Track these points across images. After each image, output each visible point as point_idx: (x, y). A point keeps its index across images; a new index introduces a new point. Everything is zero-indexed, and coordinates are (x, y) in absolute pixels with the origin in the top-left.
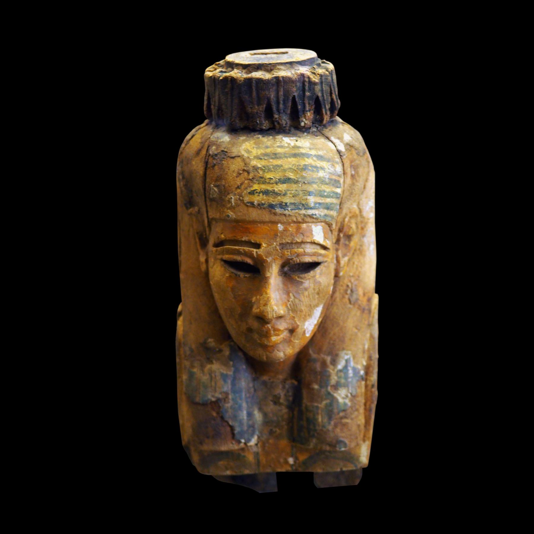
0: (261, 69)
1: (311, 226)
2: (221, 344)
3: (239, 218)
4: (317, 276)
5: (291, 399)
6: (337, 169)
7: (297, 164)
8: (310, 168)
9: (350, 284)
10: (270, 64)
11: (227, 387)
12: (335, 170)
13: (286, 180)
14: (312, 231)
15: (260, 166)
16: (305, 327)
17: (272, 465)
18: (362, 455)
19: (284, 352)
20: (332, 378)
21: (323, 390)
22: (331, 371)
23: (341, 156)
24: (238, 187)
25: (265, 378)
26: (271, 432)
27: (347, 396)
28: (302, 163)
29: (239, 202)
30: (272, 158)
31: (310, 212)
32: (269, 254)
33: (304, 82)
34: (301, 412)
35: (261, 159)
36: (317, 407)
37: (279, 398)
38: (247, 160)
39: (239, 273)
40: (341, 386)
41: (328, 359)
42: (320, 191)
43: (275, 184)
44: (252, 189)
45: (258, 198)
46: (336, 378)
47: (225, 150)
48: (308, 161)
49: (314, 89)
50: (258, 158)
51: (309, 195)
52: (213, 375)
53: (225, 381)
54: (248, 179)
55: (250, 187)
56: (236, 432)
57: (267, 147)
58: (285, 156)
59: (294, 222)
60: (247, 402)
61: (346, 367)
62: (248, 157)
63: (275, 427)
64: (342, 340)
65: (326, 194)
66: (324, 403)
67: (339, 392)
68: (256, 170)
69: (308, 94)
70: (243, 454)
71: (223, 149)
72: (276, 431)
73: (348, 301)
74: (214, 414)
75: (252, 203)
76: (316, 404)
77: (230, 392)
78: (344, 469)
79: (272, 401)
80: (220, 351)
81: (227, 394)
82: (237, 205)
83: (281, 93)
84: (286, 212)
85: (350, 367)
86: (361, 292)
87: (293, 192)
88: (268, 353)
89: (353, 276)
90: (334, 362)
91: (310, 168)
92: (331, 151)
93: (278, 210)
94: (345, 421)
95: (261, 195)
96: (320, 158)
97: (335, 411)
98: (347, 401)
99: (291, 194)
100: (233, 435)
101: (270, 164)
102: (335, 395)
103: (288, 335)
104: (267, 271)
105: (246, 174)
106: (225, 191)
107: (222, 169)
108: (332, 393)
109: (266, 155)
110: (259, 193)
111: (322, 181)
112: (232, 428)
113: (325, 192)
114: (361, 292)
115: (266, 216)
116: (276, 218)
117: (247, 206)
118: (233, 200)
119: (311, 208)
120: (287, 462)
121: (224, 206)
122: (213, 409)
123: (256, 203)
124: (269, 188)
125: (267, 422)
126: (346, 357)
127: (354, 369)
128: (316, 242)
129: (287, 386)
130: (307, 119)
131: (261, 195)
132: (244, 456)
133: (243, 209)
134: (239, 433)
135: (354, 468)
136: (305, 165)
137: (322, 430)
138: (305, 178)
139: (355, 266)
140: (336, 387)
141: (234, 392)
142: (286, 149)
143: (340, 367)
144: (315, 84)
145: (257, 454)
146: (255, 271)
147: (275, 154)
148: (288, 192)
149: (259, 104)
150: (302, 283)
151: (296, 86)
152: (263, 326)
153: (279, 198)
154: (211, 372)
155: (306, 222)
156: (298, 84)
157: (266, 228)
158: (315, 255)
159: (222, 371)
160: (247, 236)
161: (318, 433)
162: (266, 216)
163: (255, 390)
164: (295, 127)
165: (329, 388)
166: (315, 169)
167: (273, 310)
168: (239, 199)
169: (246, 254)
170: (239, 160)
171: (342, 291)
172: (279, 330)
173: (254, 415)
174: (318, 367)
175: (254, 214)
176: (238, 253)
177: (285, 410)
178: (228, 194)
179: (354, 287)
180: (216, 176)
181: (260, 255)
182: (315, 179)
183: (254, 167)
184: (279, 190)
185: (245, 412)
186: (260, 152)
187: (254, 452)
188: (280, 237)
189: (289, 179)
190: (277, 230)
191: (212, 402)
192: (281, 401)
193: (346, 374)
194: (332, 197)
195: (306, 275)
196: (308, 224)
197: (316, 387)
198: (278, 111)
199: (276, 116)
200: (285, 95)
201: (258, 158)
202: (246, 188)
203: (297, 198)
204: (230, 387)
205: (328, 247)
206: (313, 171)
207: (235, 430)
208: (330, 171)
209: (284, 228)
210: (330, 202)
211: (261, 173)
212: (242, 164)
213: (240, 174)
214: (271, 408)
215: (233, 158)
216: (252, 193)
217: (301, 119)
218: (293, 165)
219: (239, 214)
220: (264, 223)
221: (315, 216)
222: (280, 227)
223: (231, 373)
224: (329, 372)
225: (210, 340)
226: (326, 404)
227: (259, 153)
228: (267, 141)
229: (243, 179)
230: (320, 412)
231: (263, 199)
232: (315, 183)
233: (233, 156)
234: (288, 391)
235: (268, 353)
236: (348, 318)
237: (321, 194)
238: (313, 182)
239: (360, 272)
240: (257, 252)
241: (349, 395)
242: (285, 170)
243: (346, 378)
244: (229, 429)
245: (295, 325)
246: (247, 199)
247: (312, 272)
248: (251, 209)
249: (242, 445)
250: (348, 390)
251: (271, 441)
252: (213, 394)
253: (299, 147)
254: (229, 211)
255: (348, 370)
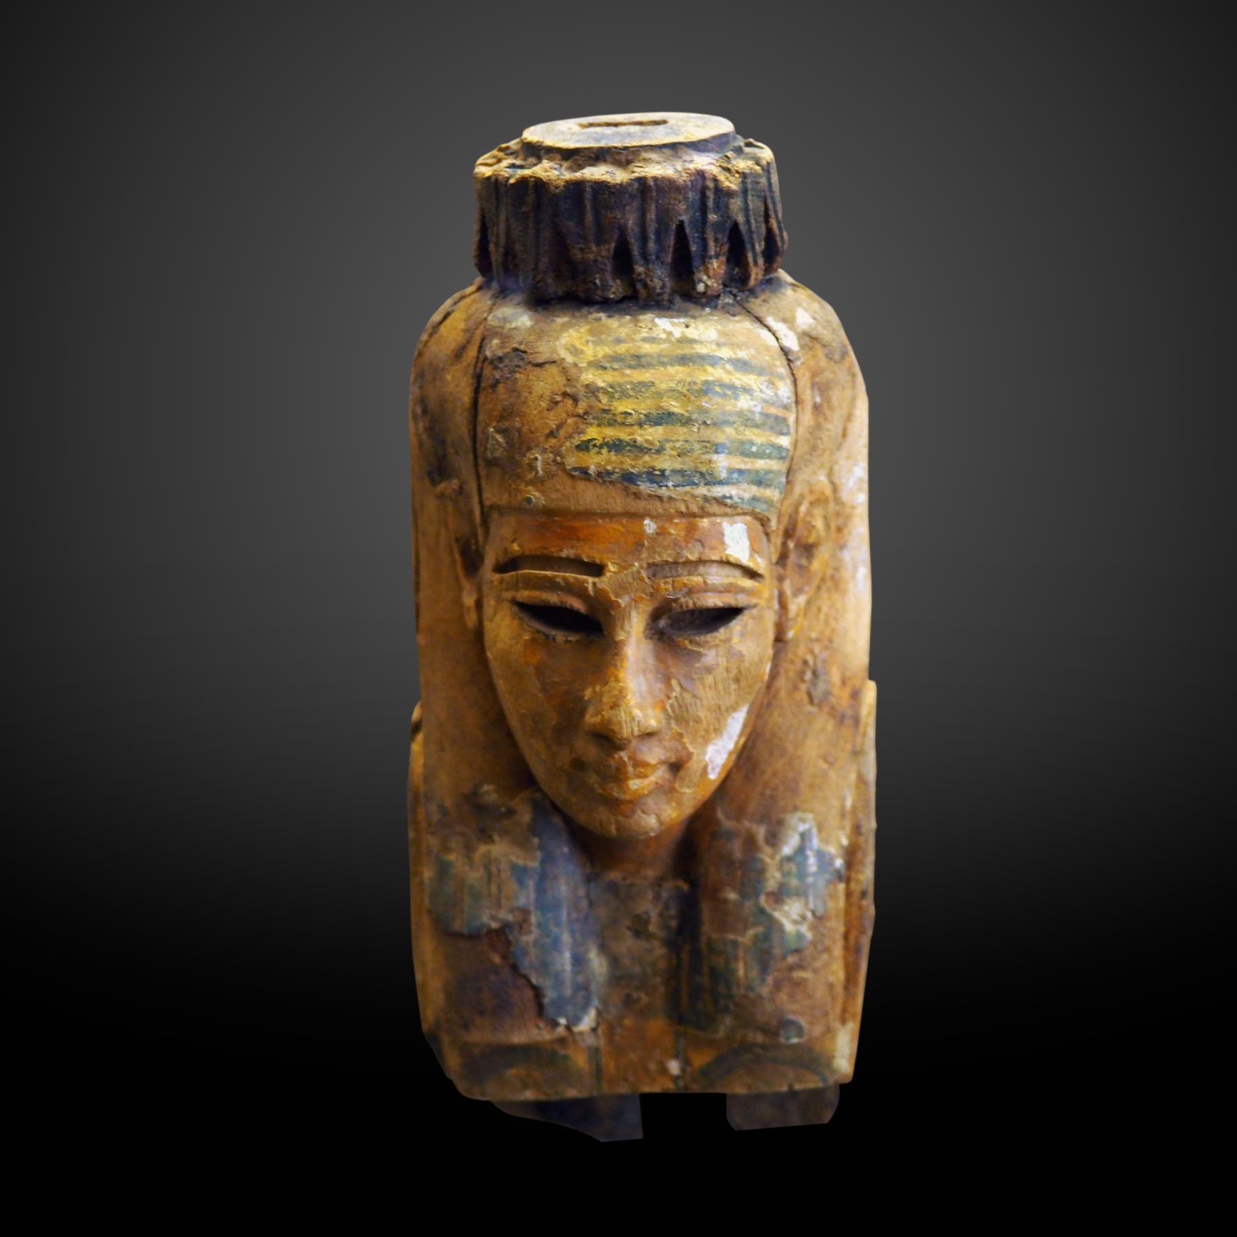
0: (605, 161)
1: (720, 524)
2: (512, 797)
3: (553, 506)
4: (735, 640)
5: (674, 923)
6: (780, 393)
7: (689, 380)
8: (718, 389)
9: (810, 658)
10: (626, 148)
11: (526, 897)
12: (776, 395)
13: (663, 418)
14: (723, 534)
15: (601, 384)
16: (707, 758)
17: (631, 1078)
18: (838, 1054)
19: (658, 816)
20: (768, 875)
21: (749, 904)
22: (767, 860)
23: (789, 361)
24: (552, 434)
25: (614, 875)
26: (628, 1002)
27: (804, 918)
28: (700, 377)
29: (554, 468)
30: (630, 367)
31: (718, 491)
32: (623, 588)
33: (704, 190)
34: (696, 955)
35: (605, 368)
36: (735, 944)
37: (646, 922)
38: (573, 371)
39: (553, 632)
40: (789, 895)
41: (761, 832)
42: (742, 443)
43: (636, 427)
44: (585, 438)
45: (597, 459)
46: (778, 875)
47: (522, 347)
48: (714, 373)
49: (727, 206)
50: (598, 365)
51: (717, 452)
52: (494, 869)
53: (521, 883)
54: (573, 416)
55: (579, 433)
56: (546, 1001)
57: (618, 341)
58: (661, 361)
59: (681, 514)
60: (572, 932)
61: (801, 850)
62: (575, 365)
63: (638, 989)
64: (793, 787)
65: (754, 449)
66: (751, 932)
67: (786, 908)
68: (593, 393)
69: (713, 217)
70: (562, 1052)
71: (516, 345)
72: (639, 999)
73: (806, 698)
74: (497, 959)
75: (584, 471)
76: (731, 937)
77: (532, 909)
78: (797, 1087)
79: (629, 928)
80: (511, 813)
81: (525, 912)
82: (550, 476)
83: (652, 216)
84: (663, 492)
85: (811, 849)
86: (836, 677)
87: (678, 445)
88: (621, 818)
89: (817, 640)
90: (774, 839)
91: (718, 389)
92: (768, 349)
93: (645, 487)
94: (798, 974)
95: (604, 451)
96: (742, 365)
97: (777, 951)
98: (804, 929)
99: (673, 448)
100: (540, 1007)
101: (626, 379)
102: (777, 914)
103: (668, 776)
104: (618, 629)
105: (569, 402)
106: (522, 443)
107: (513, 390)
108: (769, 910)
109: (616, 358)
110: (601, 447)
111: (747, 420)
112: (538, 992)
113: (752, 444)
114: (836, 677)
115: (617, 501)
116: (640, 505)
117: (573, 477)
118: (539, 464)
119: (721, 483)
120: (664, 1071)
121: (519, 477)
122: (494, 948)
123: (592, 470)
124: (624, 435)
125: (618, 978)
126: (802, 827)
127: (820, 855)
128: (732, 560)
129: (665, 895)
130: (711, 276)
131: (604, 451)
132: (566, 1057)
133: (562, 485)
134: (555, 1003)
135: (821, 1085)
136: (706, 382)
137: (746, 996)
138: (706, 411)
139: (822, 616)
140: (779, 896)
141: (542, 907)
142: (663, 346)
143: (787, 850)
144: (730, 194)
145: (594, 1052)
146: (592, 627)
147: (638, 357)
148: (668, 446)
149: (600, 241)
150: (699, 655)
151: (686, 199)
152: (610, 755)
153: (647, 458)
154: (488, 863)
155: (709, 515)
156: (691, 195)
157: (615, 527)
158: (729, 591)
159: (514, 859)
160: (572, 547)
161: (736, 1004)
162: (617, 501)
163: (591, 904)
164: (684, 295)
165: (762, 899)
166: (729, 393)
167: (633, 719)
168: (554, 461)
169: (570, 589)
170: (553, 370)
171: (792, 674)
172: (646, 765)
173: (589, 960)
174: (737, 849)
175: (588, 496)
176: (552, 585)
177: (660, 951)
178: (529, 449)
179: (819, 664)
180: (499, 407)
181: (602, 590)
182: (730, 414)
183: (587, 386)
184: (647, 441)
185: (567, 955)
186: (602, 351)
187: (589, 1048)
188: (648, 549)
189: (670, 414)
190: (643, 533)
191: (491, 932)
192: (652, 928)
193: (802, 866)
194: (769, 457)
195: (709, 637)
196: (713, 519)
197: (732, 896)
198: (645, 256)
199: (640, 269)
200: (659, 221)
201: (598, 365)
202: (570, 437)
203: (688, 459)
204: (532, 896)
205: (761, 571)
206: (724, 396)
207: (544, 996)
208: (764, 396)
209: (659, 528)
210: (765, 467)
211: (604, 400)
212: (561, 380)
213: (556, 403)
214: (627, 944)
215: (540, 365)
216: (584, 447)
217: (697, 276)
218: (679, 382)
219: (554, 496)
220: (610, 515)
221: (729, 501)
222: (650, 526)
223: (534, 864)
224: (762, 861)
225: (486, 788)
226: (756, 936)
227: (600, 355)
228: (619, 326)
229: (564, 415)
230: (741, 953)
231: (609, 462)
232: (730, 424)
233: (540, 360)
234: (667, 907)
235: (621, 818)
236: (806, 736)
237: (743, 450)
238: (726, 422)
239: (833, 631)
240: (594, 584)
241: (809, 915)
242: (659, 395)
243: (802, 875)
244: (529, 994)
245: (684, 754)
246: (571, 461)
247: (722, 630)
248: (581, 485)
249: (561, 1031)
250: (807, 904)
251: (628, 1022)
252: (494, 912)
253: (692, 341)
254: (530, 488)
255: (806, 858)
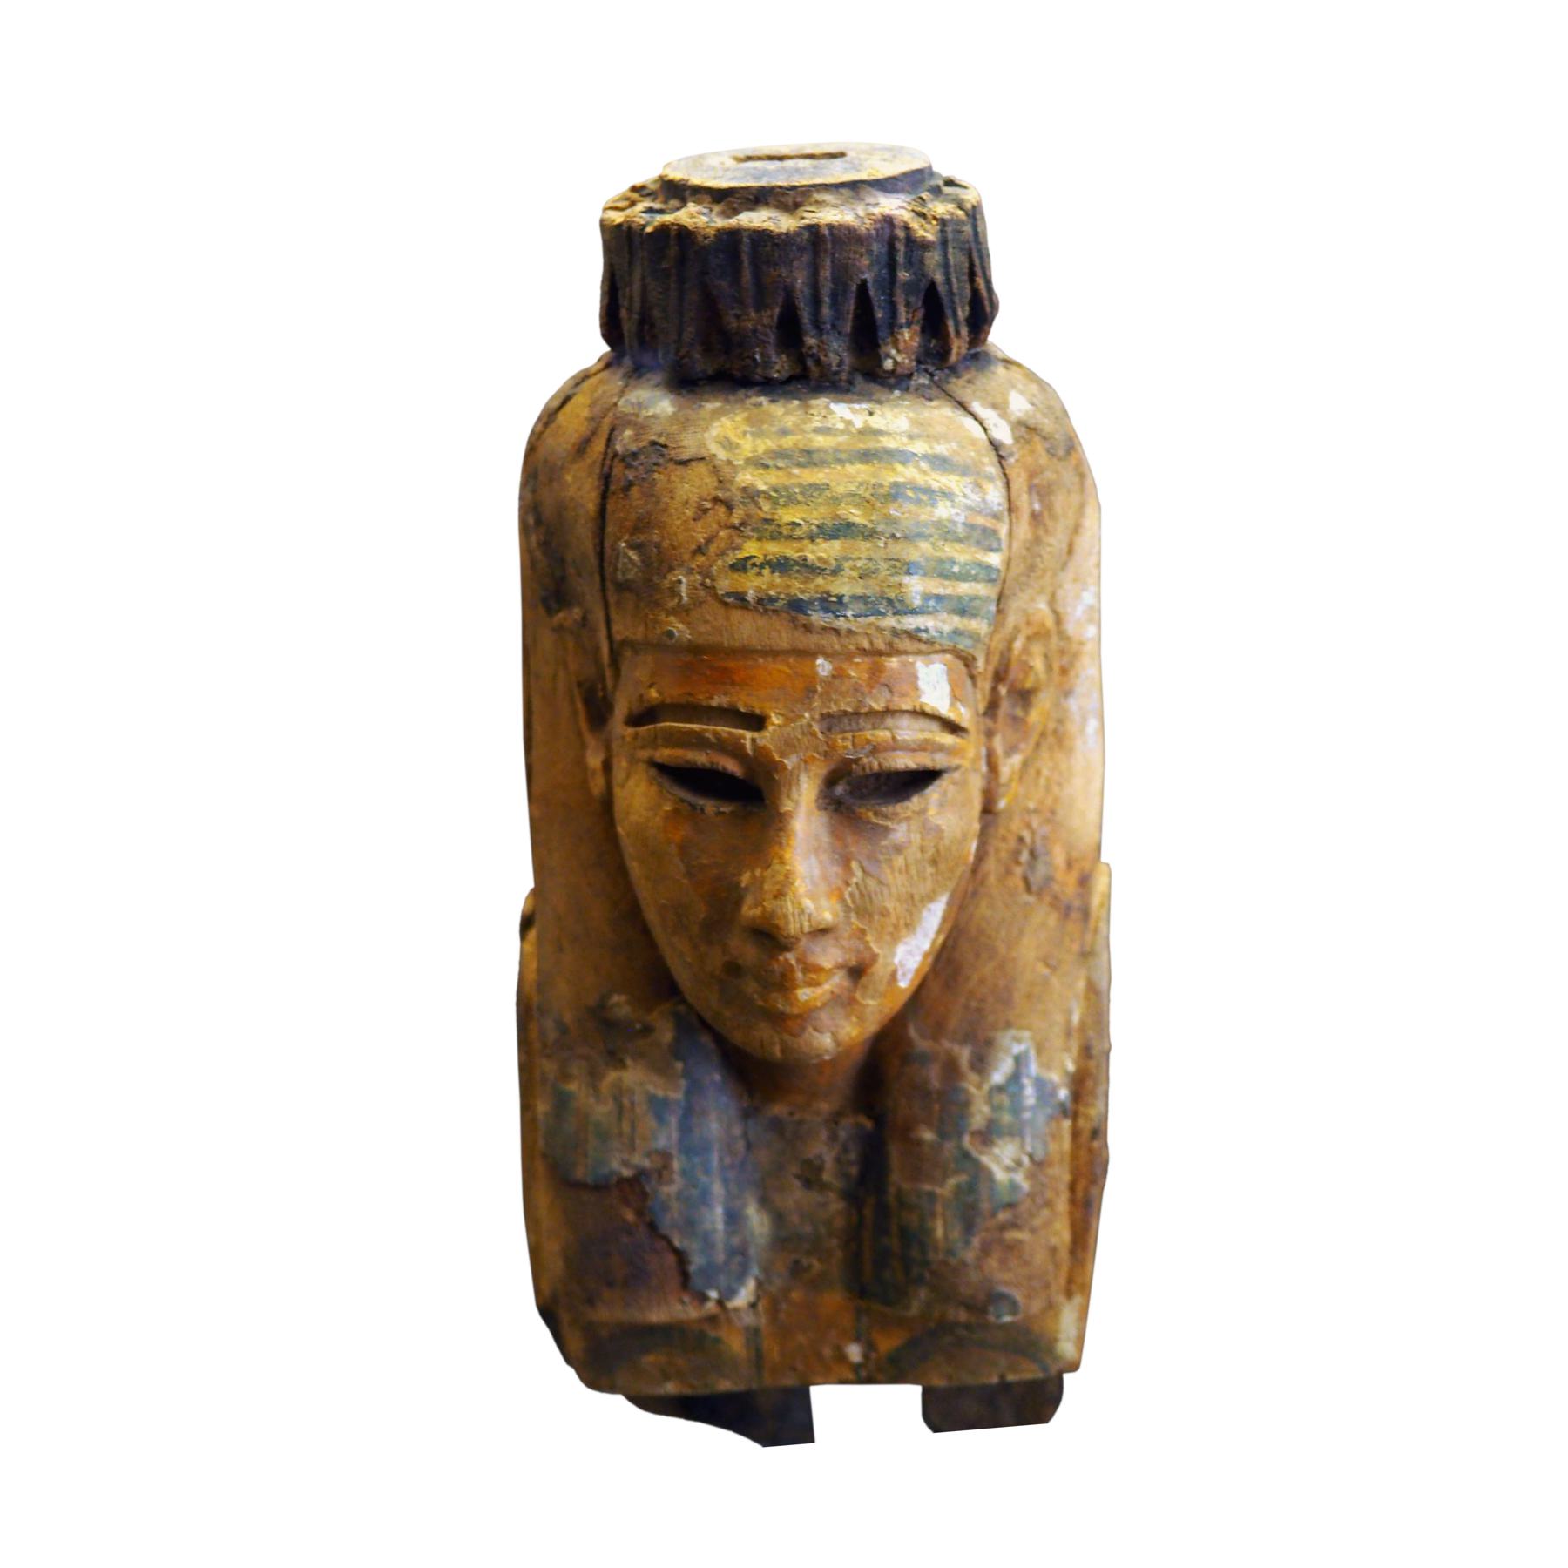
0: (767, 204)
1: (913, 664)
2: (649, 1010)
3: (701, 641)
4: (932, 811)
5: (854, 1170)
6: (989, 498)
7: (873, 481)
8: (910, 493)
9: (1026, 834)
10: (794, 188)
11: (667, 1137)
12: (984, 500)
13: (841, 530)
14: (916, 677)
15: (762, 487)
16: (896, 961)
17: (800, 1367)
18: (1062, 1336)
19: (834, 1035)
20: (974, 1109)
21: (949, 1146)
22: (973, 1090)
23: (1000, 457)
24: (699, 550)
25: (778, 1109)
26: (796, 1270)
27: (1019, 1163)
28: (888, 478)
29: (702, 593)
30: (799, 465)
31: (911, 622)
32: (789, 746)
33: (892, 240)
34: (883, 1210)
35: (767, 467)
36: (932, 1196)
37: (819, 1169)
38: (727, 470)
39: (701, 802)
40: (1001, 1134)
41: (964, 1054)
42: (941, 561)
43: (806, 542)
44: (741, 555)
45: (757, 582)
46: (986, 1109)
47: (662, 440)
48: (905, 473)
49: (922, 261)
50: (758, 463)
51: (908, 573)
52: (626, 1102)
53: (660, 1119)
54: (727, 527)
55: (734, 549)
56: (692, 1268)
57: (784, 432)
58: (838, 458)
59: (864, 652)
60: (725, 1182)
61: (1015, 1077)
62: (729, 462)
63: (809, 1253)
64: (1005, 998)
65: (956, 569)
66: (952, 1182)
67: (996, 1151)
68: (752, 498)
69: (903, 275)
70: (712, 1334)
71: (654, 438)
72: (810, 1266)
73: (1021, 885)
74: (630, 1216)
75: (741, 597)
76: (927, 1187)
77: (674, 1152)
78: (1011, 1378)
79: (798, 1177)
80: (647, 1030)
81: (666, 1156)
82: (697, 603)
83: (826, 273)
84: (841, 623)
85: (1028, 1076)
86: (1059, 858)
87: (859, 564)
88: (787, 1037)
89: (1036, 811)
90: (981, 1064)
91: (910, 493)
92: (973, 442)
93: (817, 617)
94: (1012, 1235)
95: (766, 571)
96: (941, 463)
97: (985, 1206)
98: (1019, 1177)
99: (853, 568)
100: (685, 1277)
101: (794, 481)
102: (985, 1159)
103: (847, 983)
104: (784, 797)
105: (722, 510)
106: (662, 562)
107: (650, 495)
108: (975, 1154)
109: (781, 454)
110: (762, 566)
111: (947, 533)
112: (681, 1257)
113: (954, 562)
114: (1059, 858)
115: (782, 635)
116: (812, 641)
117: (726, 604)
118: (683, 589)
119: (914, 612)
121: (657, 604)
122: (626, 1202)
123: (751, 595)
124: (791, 551)
125: (783, 1239)
126: (1017, 1049)
127: (1040, 1084)
128: (928, 710)
129: (842, 1134)
130: (902, 349)
131: (766, 571)
132: (717, 1340)
133: (713, 615)
134: (703, 1271)
135: (1040, 1375)
136: (895, 485)
137: (945, 1263)
138: (895, 521)
139: (1042, 781)
140: (987, 1136)
141: (687, 1150)
142: (841, 439)
143: (998, 1077)
144: (925, 246)
145: (753, 1334)
146: (750, 795)
147: (809, 452)
148: (847, 565)
149: (760, 306)
150: (887, 830)
151: (870, 252)
152: (773, 957)
153: (820, 580)
154: (619, 1094)
155: (899, 653)
156: (875, 247)
157: (780, 668)
158: (924, 750)
159: (651, 1088)
160: (726, 694)
161: (933, 1273)
162: (782, 635)
163: (749, 1146)
164: (868, 374)
165: (966, 1140)
166: (924, 498)
167: (803, 911)
168: (703, 584)
169: (722, 746)
170: (701, 468)
171: (1004, 855)
172: (818, 969)
173: (747, 1217)
174: (934, 1076)
175: (746, 629)
176: (700, 742)
177: (836, 1205)
178: (671, 569)
179: (1039, 842)
180: (633, 516)
181: (764, 748)
182: (926, 525)
183: (744, 489)
184: (820, 559)
185: (719, 1211)
186: (764, 445)
187: (747, 1329)
188: (821, 695)
189: (850, 525)
190: (815, 675)
191: (622, 1181)
192: (827, 1177)
193: (1017, 1097)
194: (975, 579)
195: (899, 808)
196: (904, 657)
197: (928, 1135)
198: (817, 325)
199: (811, 341)
200: (835, 280)
201: (758, 463)
202: (723, 553)
203: (872, 582)
204: (675, 1135)
205: (964, 724)
206: (918, 502)
207: (689, 1263)
208: (969, 502)
209: (835, 669)
210: (970, 592)
211: (766, 507)
212: (711, 482)
213: (705, 511)
214: (795, 1197)
215: (685, 463)
216: (741, 566)
217: (883, 350)
218: (861, 484)
219: (702, 629)
220: (774, 653)
221: (924, 635)
222: (823, 667)
223: (677, 1096)
224: (966, 1091)
225: (616, 998)
226: (958, 1186)
227: (761, 450)
228: (784, 413)
229: (715, 526)
230: (939, 1208)
231: (772, 586)
232: (926, 537)
233: (685, 457)
234: (845, 1150)
235: (787, 1037)
236: (1021, 933)
237: (942, 570)
238: (920, 535)
239: (1056, 800)
240: (753, 740)
241: (1026, 1160)
242: (836, 501)
243: (1017, 1109)
244: (671, 1259)
245: (867, 956)
246: (724, 584)
247: (915, 799)
248: (736, 615)
249: (711, 1306)
250: (1022, 1146)
251: (795, 1295)
252: (626, 1156)
253: (877, 433)
254: (672, 618)
255: (1021, 1087)
